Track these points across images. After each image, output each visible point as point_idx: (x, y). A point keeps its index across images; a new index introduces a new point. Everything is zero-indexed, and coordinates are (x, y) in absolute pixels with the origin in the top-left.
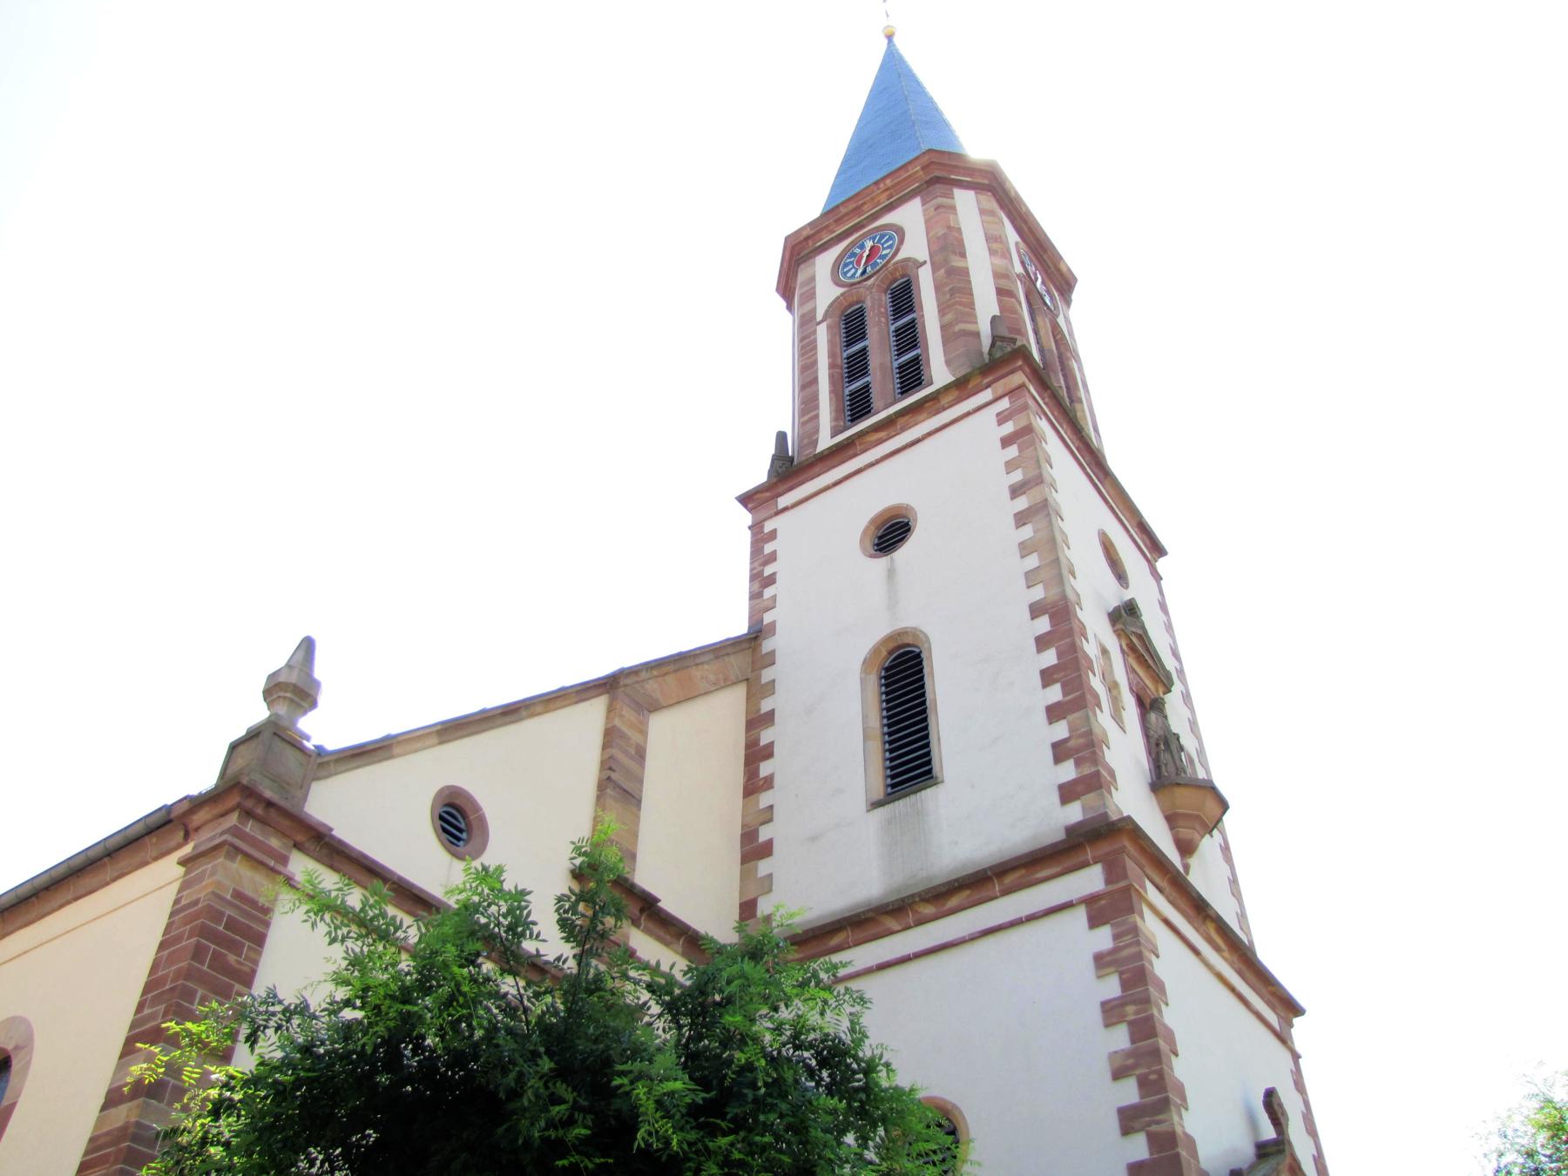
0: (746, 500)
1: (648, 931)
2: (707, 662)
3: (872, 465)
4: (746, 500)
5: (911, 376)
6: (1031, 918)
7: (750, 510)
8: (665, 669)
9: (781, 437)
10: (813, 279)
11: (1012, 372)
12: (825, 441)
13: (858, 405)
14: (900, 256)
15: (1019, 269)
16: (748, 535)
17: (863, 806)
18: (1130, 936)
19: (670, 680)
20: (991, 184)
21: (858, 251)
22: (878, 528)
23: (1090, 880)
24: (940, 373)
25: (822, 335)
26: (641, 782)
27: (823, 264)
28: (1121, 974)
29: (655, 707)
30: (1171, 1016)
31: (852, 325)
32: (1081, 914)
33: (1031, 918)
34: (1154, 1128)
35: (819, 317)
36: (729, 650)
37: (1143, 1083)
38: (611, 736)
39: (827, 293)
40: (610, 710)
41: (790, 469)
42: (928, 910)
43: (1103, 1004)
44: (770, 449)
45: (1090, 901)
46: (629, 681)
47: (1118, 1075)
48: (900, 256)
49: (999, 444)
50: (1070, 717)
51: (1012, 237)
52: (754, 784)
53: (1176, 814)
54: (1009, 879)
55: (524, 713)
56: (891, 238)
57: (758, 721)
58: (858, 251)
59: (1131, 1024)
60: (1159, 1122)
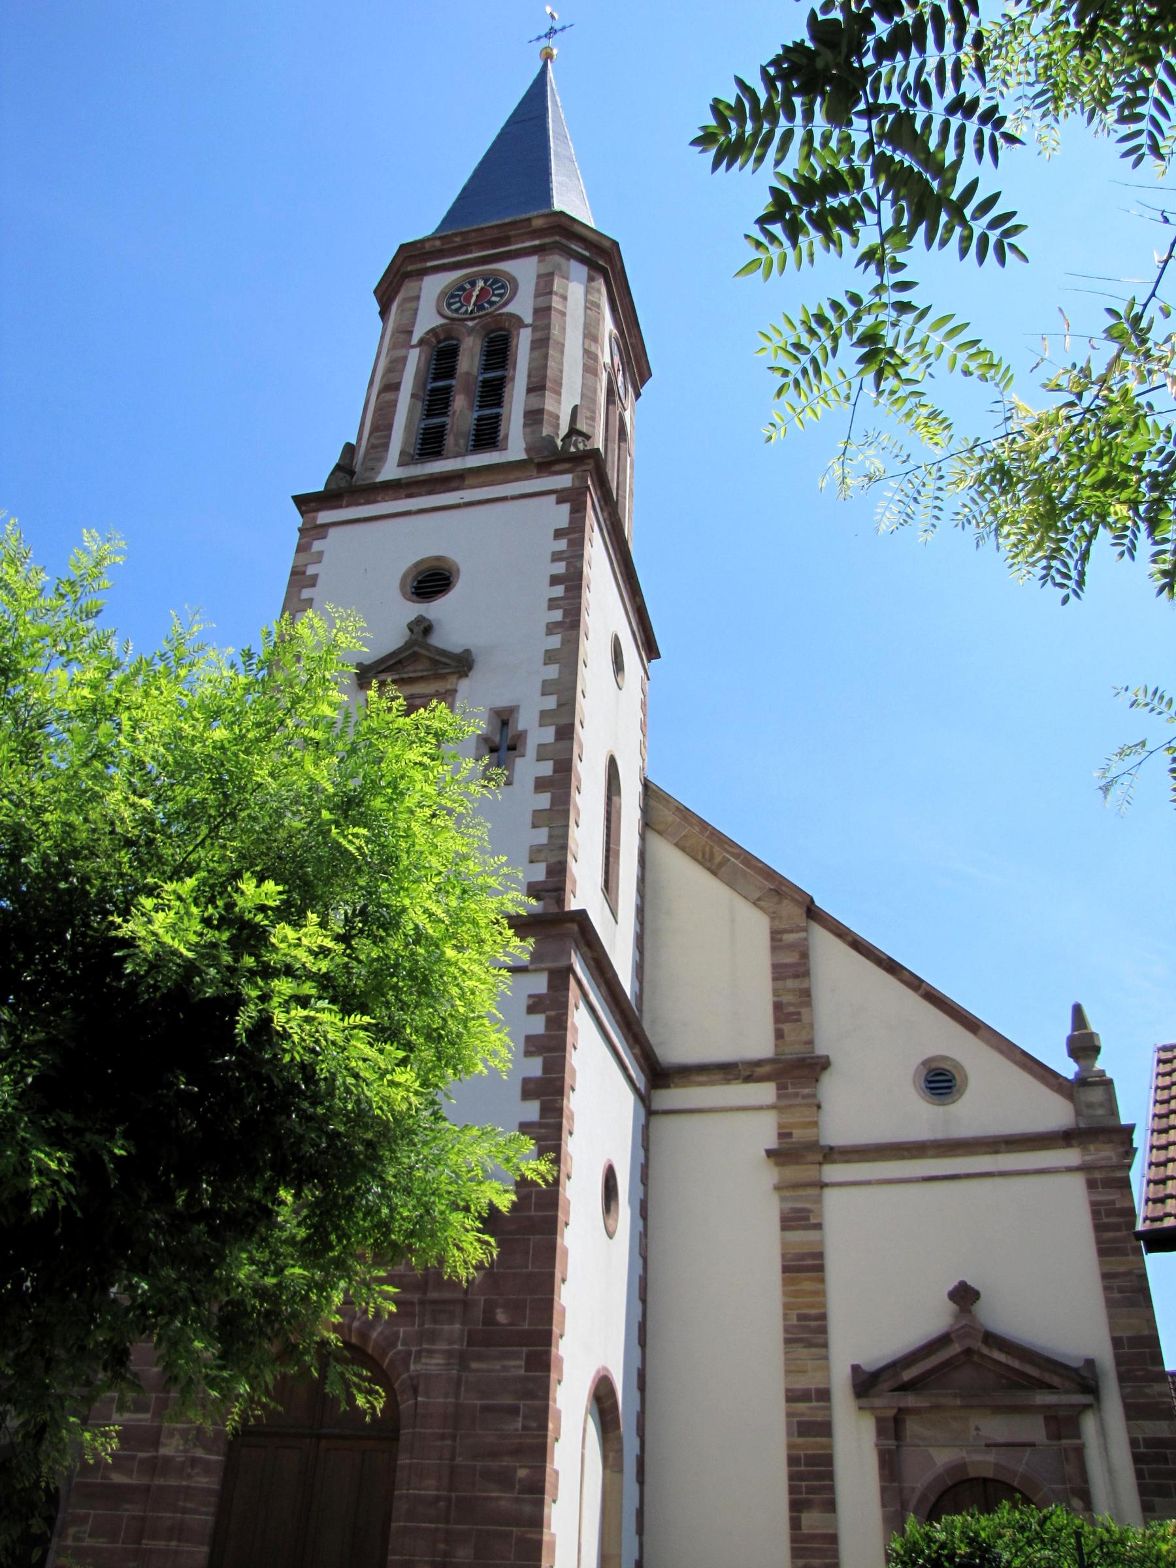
0: (304, 502)
4: (304, 502)
5: (487, 435)
7: (302, 514)
10: (417, 298)
12: (390, 470)
13: (430, 443)
14: (508, 309)
15: (608, 360)
18: (559, 1023)
20: (602, 259)
21: (468, 286)
22: (415, 578)
23: (564, 481)
24: (515, 448)
25: (414, 358)
27: (433, 286)
30: (584, 707)
31: (442, 355)
32: (553, 498)
35: (415, 341)
39: (427, 319)
41: (352, 483)
43: (552, 576)
44: (335, 458)
48: (508, 309)
49: (548, 580)
50: (549, 1013)
51: (608, 326)
56: (503, 287)
58: (468, 286)
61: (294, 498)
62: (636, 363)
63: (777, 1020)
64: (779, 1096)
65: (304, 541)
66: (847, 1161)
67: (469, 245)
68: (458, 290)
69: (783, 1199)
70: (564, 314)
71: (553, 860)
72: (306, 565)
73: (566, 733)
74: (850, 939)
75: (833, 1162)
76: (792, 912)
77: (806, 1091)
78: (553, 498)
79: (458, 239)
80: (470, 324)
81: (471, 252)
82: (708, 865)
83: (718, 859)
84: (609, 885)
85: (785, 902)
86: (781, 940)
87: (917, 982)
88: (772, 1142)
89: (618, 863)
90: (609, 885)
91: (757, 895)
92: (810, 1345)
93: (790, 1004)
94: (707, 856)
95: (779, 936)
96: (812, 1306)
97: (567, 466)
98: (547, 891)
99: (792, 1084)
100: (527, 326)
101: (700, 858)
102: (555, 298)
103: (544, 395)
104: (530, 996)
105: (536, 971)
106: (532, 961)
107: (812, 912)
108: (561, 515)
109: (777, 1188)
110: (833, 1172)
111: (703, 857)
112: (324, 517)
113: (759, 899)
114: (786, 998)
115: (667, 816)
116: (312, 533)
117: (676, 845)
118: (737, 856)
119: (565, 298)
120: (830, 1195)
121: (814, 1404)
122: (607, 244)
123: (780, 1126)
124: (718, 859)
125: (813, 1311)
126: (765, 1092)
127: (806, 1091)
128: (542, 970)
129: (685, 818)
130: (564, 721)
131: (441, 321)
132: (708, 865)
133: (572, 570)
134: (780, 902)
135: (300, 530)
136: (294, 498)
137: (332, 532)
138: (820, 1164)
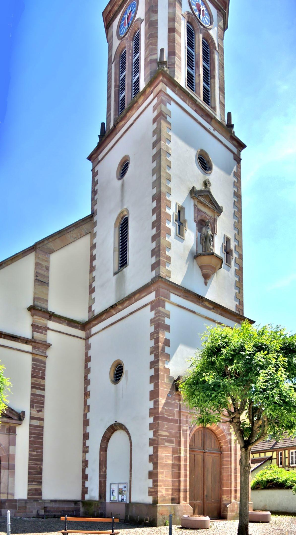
1: (54, 321)
2: (73, 230)
3: (121, 137)
6: (140, 309)
8: (55, 238)
9: (103, 124)
11: (158, 83)
16: (91, 173)
17: (112, 274)
19: (58, 241)
22: (122, 166)
23: (151, 297)
26: (48, 277)
28: (155, 325)
29: (52, 251)
33: (140, 309)
34: (156, 367)
36: (82, 224)
37: (155, 355)
38: (37, 265)
40: (37, 257)
42: (120, 307)
45: (151, 303)
46: (40, 245)
47: (151, 353)
52: (92, 269)
53: (202, 266)
54: (137, 296)
55: (4, 265)
57: (93, 247)
59: (155, 339)
60: (156, 366)
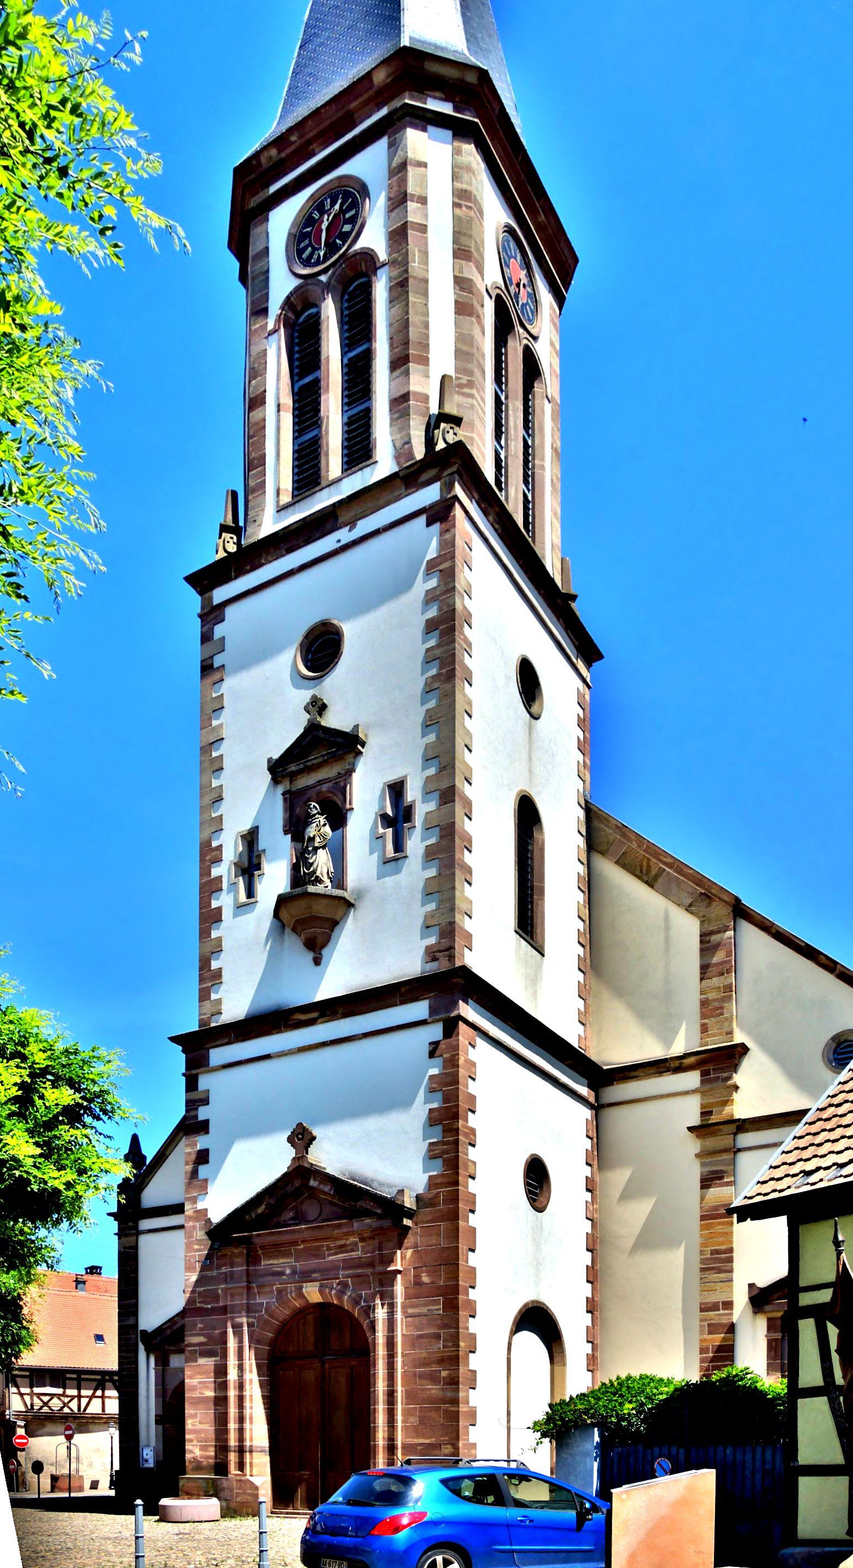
14: (359, 245)
21: (316, 215)
23: (430, 494)
48: (359, 245)
61: (189, 579)
62: (544, 243)
63: (703, 1016)
64: (702, 1082)
65: (205, 628)
66: (758, 1130)
67: (309, 142)
68: (306, 226)
69: (703, 1165)
70: (423, 228)
71: (444, 923)
72: (212, 657)
73: (447, 795)
74: (774, 931)
75: (747, 1131)
76: (720, 911)
77: (725, 1075)
78: (423, 519)
79: (293, 138)
80: (323, 278)
81: (314, 155)
82: (645, 878)
83: (654, 872)
84: (528, 923)
85: (714, 904)
86: (709, 942)
87: (832, 965)
88: (695, 1120)
89: (543, 899)
90: (528, 923)
91: (689, 901)
92: (720, 1271)
93: (715, 1000)
94: (644, 869)
95: (708, 938)
96: (723, 1243)
97: (432, 473)
98: (440, 951)
99: (714, 1069)
100: (384, 265)
101: (638, 873)
102: (411, 206)
103: (407, 373)
104: (430, 1044)
105: (433, 1022)
106: (431, 1014)
107: (740, 911)
108: (427, 540)
109: (697, 1156)
110: (746, 1139)
111: (641, 872)
112: (220, 594)
113: (690, 905)
114: (712, 996)
115: (608, 833)
116: (212, 616)
117: (617, 863)
118: (670, 866)
119: (423, 200)
120: (743, 1158)
121: (721, 1312)
122: (472, 78)
123: (703, 1106)
124: (654, 872)
125: (723, 1247)
126: (692, 1079)
127: (725, 1075)
128: (438, 1021)
129: (624, 835)
130: (445, 785)
131: (298, 282)
132: (645, 878)
133: (445, 609)
134: (709, 905)
135: (200, 616)
136: (189, 579)
137: (230, 612)
138: (735, 1134)
